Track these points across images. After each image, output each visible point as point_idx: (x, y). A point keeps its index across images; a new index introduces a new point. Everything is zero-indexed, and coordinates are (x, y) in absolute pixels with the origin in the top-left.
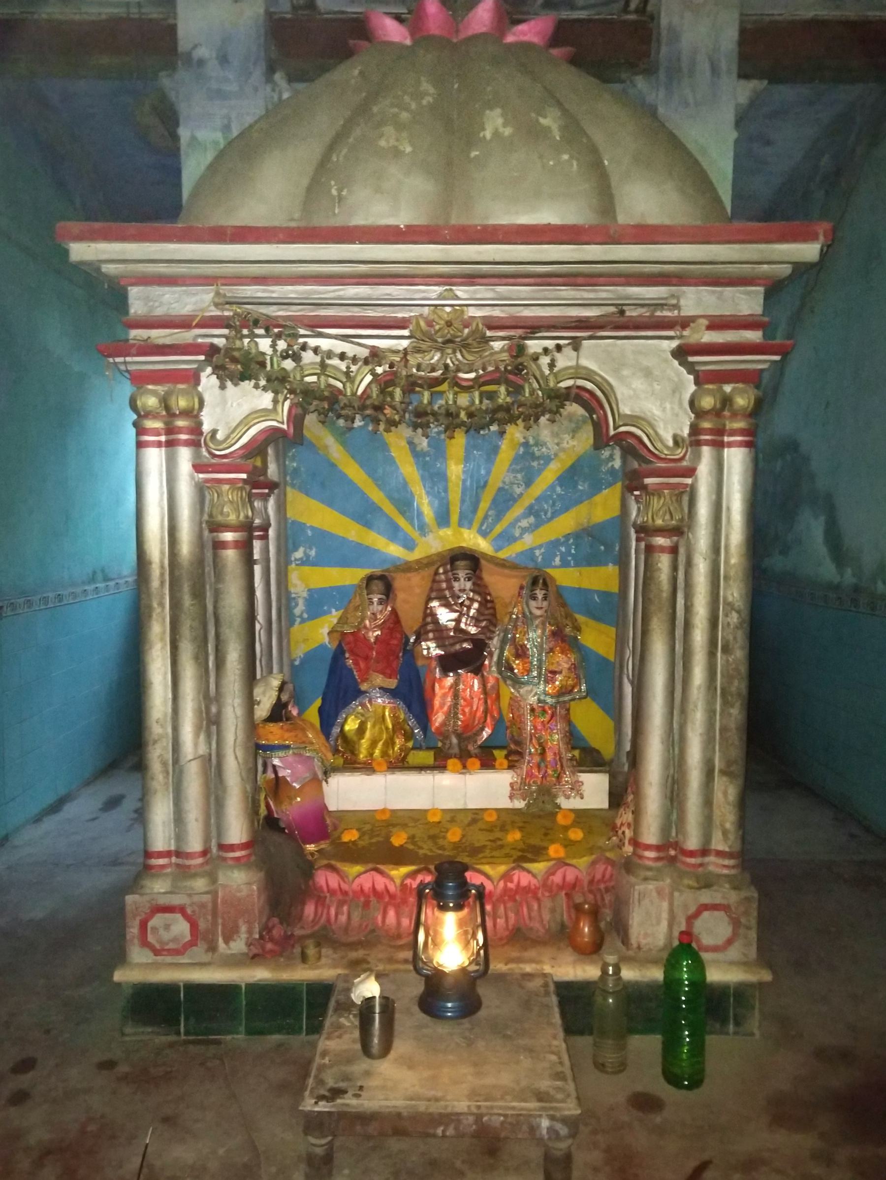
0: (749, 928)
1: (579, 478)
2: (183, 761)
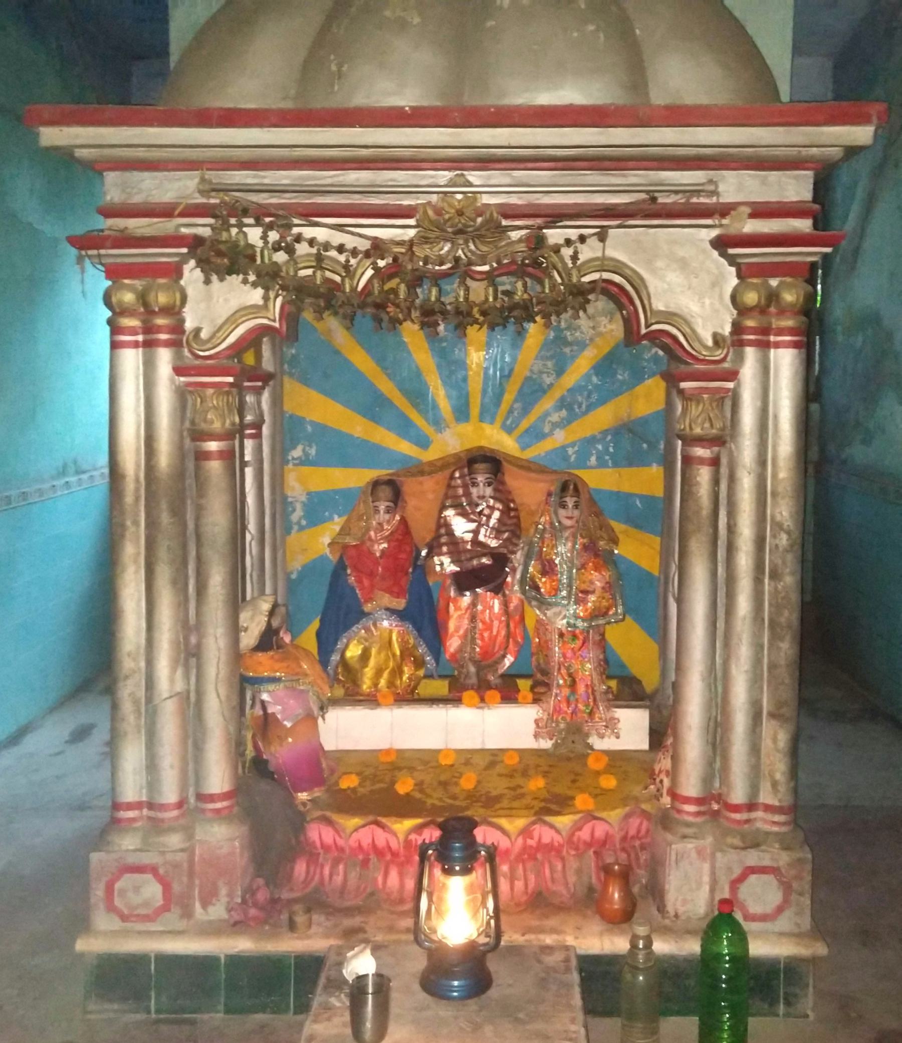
0: (801, 894)
2: (156, 701)
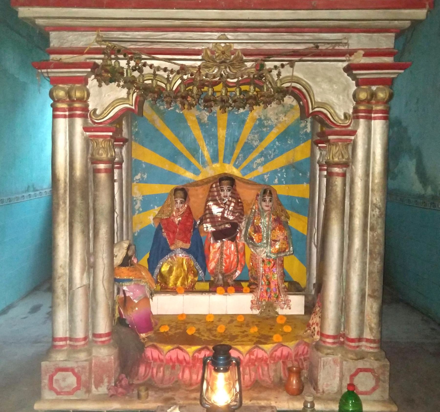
0: (384, 382)
1: (289, 136)
2: (74, 289)
